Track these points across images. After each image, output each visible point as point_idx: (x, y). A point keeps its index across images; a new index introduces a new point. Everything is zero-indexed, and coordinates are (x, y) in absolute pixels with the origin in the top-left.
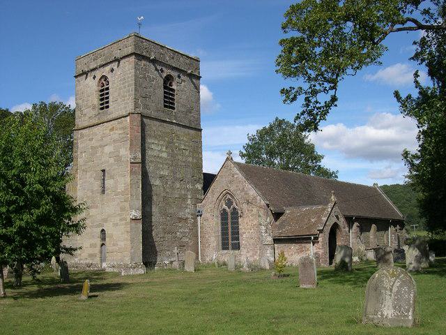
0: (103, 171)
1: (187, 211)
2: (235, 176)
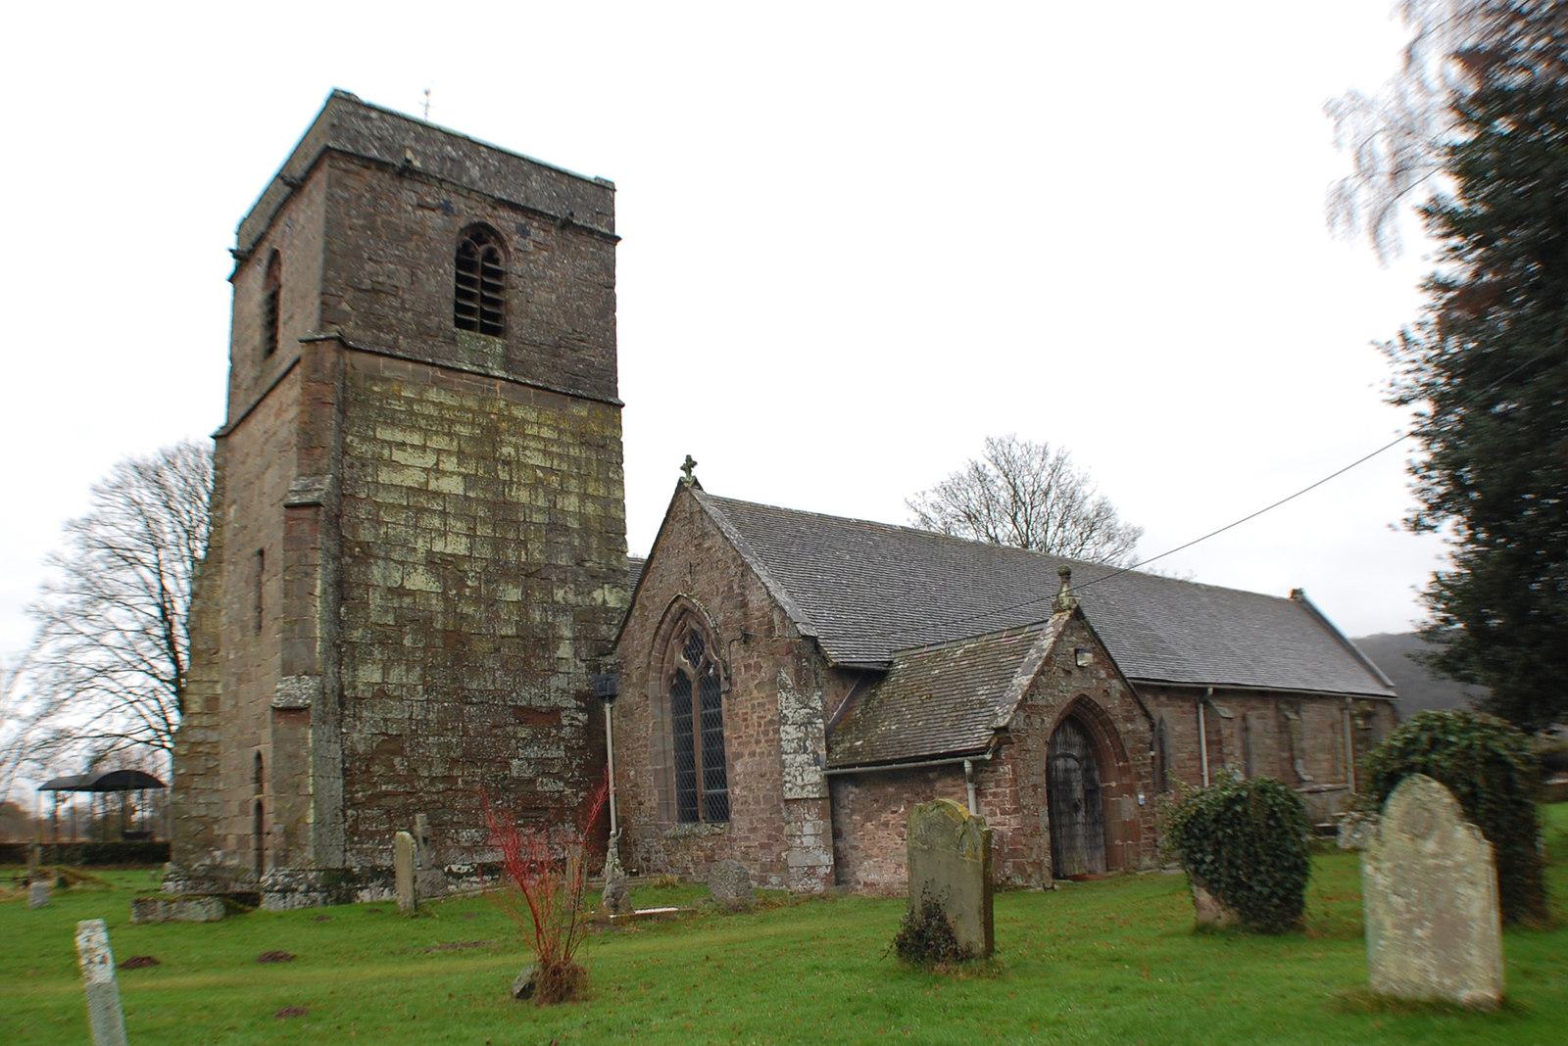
0: (261, 553)
1: (556, 682)
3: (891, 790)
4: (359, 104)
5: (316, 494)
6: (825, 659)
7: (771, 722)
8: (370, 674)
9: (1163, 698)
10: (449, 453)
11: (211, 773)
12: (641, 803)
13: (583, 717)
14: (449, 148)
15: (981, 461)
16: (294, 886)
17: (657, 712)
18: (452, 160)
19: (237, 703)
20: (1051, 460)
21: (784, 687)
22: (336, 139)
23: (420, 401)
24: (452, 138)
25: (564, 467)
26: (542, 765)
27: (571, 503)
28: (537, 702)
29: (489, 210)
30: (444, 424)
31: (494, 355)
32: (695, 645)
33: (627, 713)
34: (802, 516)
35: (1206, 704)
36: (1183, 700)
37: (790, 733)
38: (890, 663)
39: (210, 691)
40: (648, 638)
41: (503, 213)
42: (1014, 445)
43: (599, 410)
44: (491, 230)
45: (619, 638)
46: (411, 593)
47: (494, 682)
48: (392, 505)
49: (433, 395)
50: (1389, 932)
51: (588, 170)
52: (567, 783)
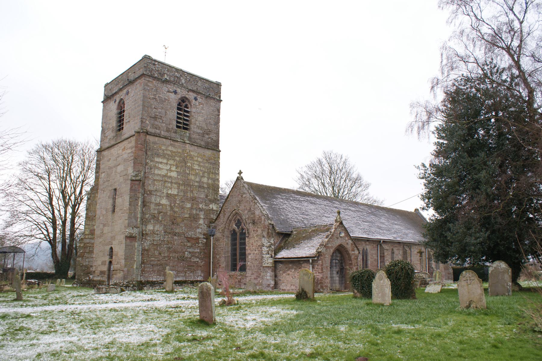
0: (115, 190)
1: (199, 230)
2: (244, 196)
3: (290, 265)
4: (152, 60)
5: (140, 177)
6: (275, 230)
7: (259, 246)
8: (150, 227)
9: (367, 243)
10: (174, 165)
11: (91, 252)
12: (220, 266)
13: (205, 240)
14: (177, 73)
15: (321, 158)
16: (129, 285)
17: (227, 240)
18: (177, 77)
19: (103, 232)
20: (343, 160)
21: (264, 237)
22: (146, 71)
23: (166, 150)
24: (177, 70)
25: (204, 169)
26: (193, 254)
27: (205, 180)
28: (193, 236)
29: (187, 92)
30: (171, 157)
31: (186, 136)
32: (239, 223)
33: (217, 240)
34: (269, 187)
35: (381, 245)
36: (374, 243)
37: (265, 249)
38: (292, 232)
39: (92, 228)
40: (225, 220)
41: (191, 93)
42: (332, 154)
43: (215, 152)
44: (187, 99)
45: (216, 219)
46: (162, 205)
47: (182, 230)
48: (158, 180)
49: (170, 148)
50: (375, 295)
51: (213, 78)
52: (200, 259)
